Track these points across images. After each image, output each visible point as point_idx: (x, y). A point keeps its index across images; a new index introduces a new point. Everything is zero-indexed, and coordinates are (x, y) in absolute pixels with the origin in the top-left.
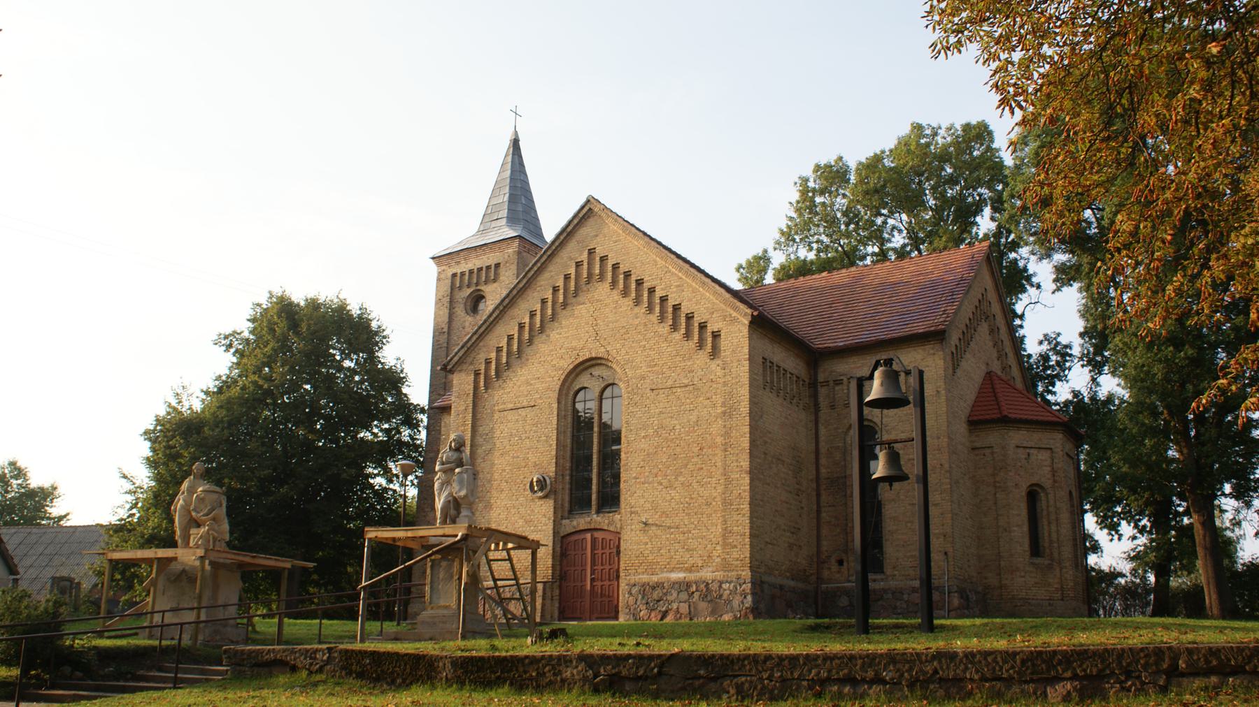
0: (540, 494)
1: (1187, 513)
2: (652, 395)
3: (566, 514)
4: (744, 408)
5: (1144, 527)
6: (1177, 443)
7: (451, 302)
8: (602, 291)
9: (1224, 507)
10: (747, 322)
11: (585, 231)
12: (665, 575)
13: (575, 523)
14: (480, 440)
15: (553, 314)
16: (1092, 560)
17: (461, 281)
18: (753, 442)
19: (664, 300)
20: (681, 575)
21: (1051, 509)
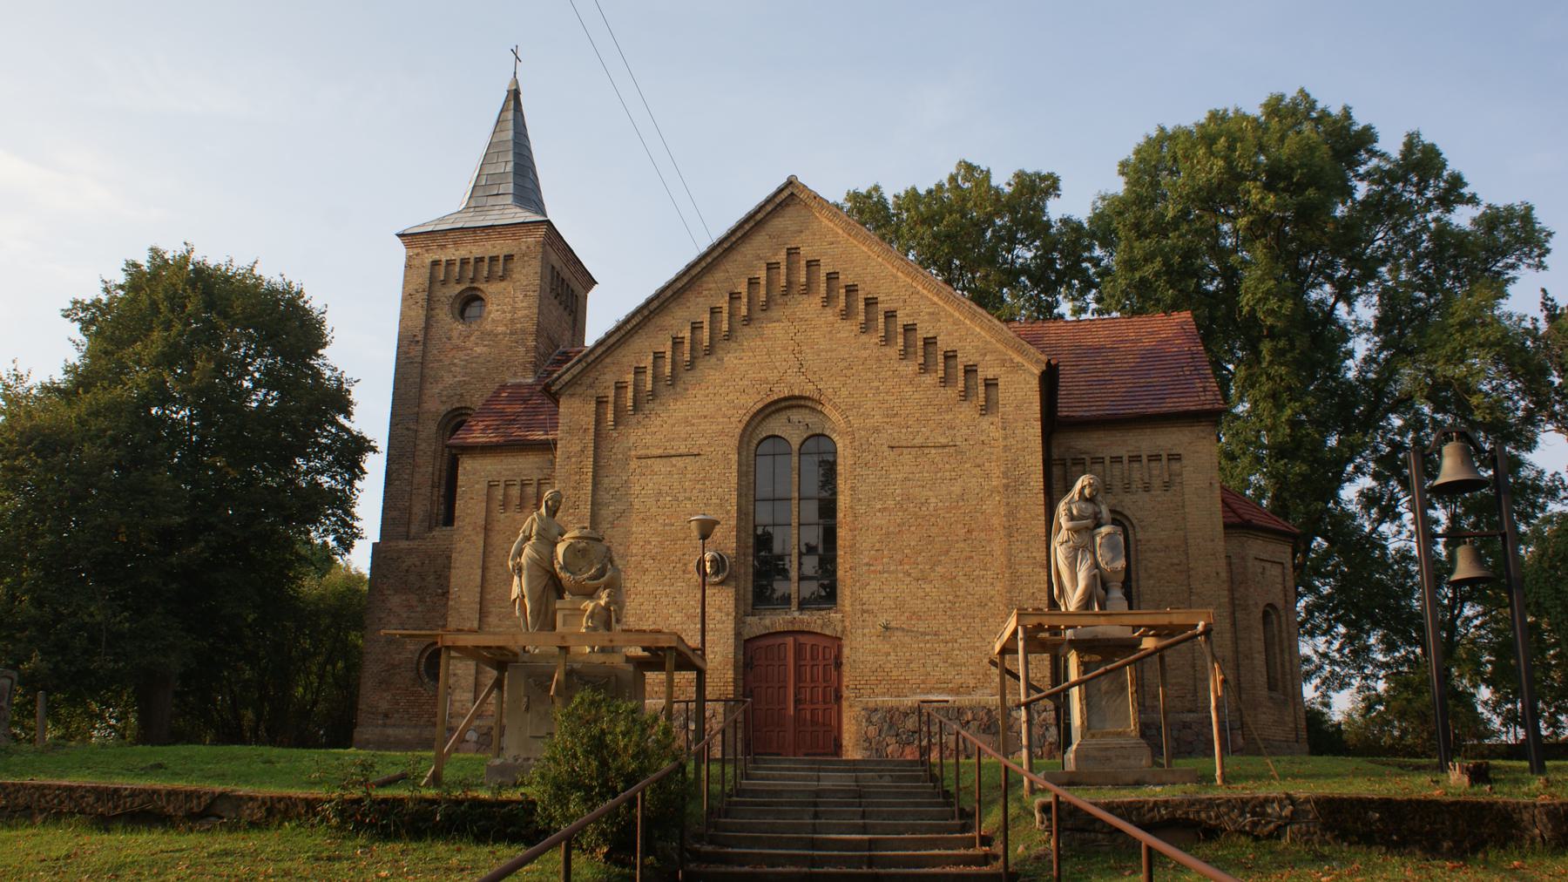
2: (893, 455)
3: (749, 609)
7: (429, 300)
10: (1037, 372)
11: (778, 223)
13: (767, 622)
14: (605, 497)
15: (730, 330)
17: (447, 273)
21: (1285, 635)
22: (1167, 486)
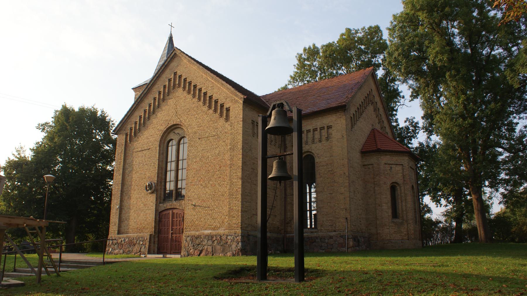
0: (150, 191)
1: (469, 194)
3: (162, 201)
4: (240, 146)
5: (451, 201)
6: (464, 163)
8: (180, 93)
9: (486, 191)
10: (242, 102)
11: (173, 64)
12: (202, 231)
13: (165, 205)
14: (127, 166)
16: (427, 215)
18: (244, 163)
19: (205, 94)
20: (209, 232)
21: (403, 195)
22: (328, 139)
